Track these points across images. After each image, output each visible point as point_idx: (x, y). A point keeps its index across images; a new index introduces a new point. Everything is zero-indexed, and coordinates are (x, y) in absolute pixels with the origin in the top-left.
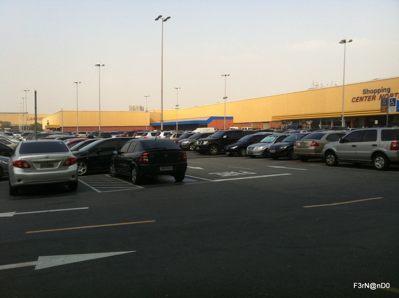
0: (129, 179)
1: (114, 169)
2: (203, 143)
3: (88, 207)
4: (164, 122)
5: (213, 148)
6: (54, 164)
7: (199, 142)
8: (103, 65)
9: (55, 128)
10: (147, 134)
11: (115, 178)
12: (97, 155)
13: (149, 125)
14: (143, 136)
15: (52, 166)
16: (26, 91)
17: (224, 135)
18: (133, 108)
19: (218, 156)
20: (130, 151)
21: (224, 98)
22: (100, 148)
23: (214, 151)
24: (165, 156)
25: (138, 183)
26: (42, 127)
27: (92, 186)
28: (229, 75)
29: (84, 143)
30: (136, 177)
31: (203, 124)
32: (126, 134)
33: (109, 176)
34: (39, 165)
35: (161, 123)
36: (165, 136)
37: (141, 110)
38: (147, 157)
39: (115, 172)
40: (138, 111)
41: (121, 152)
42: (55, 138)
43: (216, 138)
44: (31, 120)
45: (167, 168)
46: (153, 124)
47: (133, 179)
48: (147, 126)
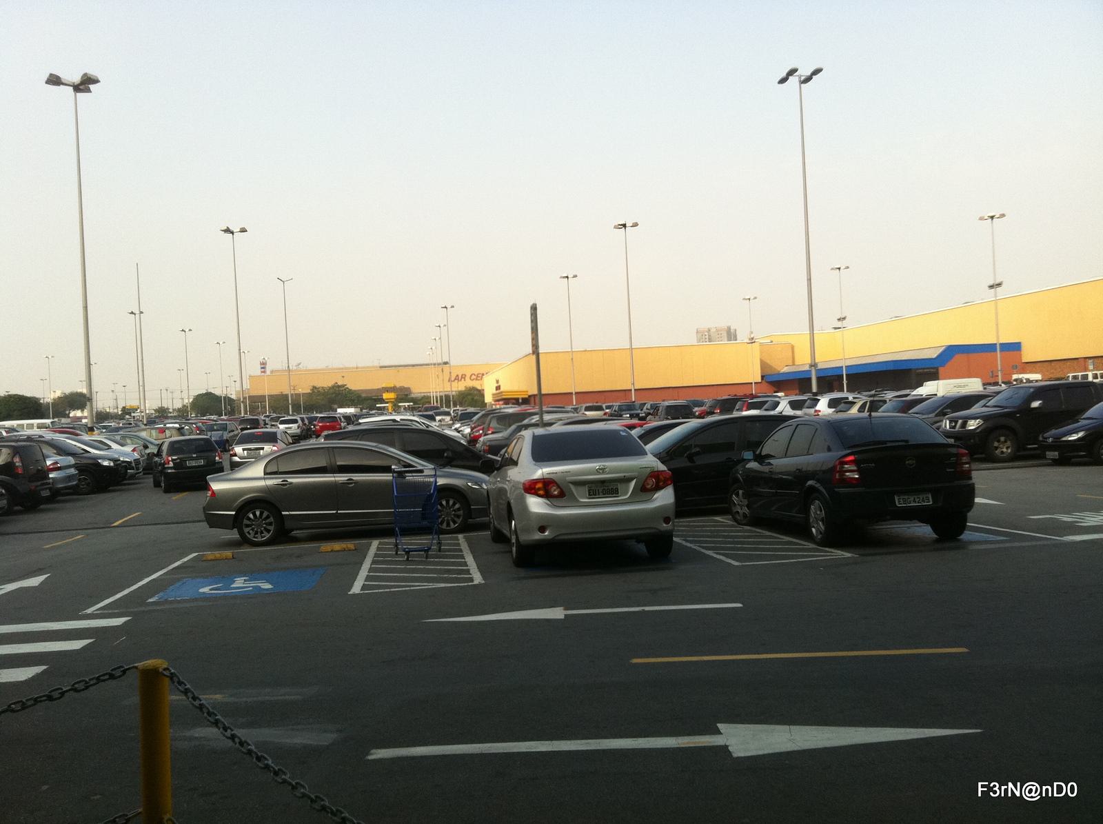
0: (800, 530)
1: (746, 502)
2: (964, 424)
3: (742, 604)
4: (820, 366)
5: (999, 441)
6: (619, 486)
7: (950, 423)
8: (635, 225)
9: (517, 400)
10: (777, 404)
11: (748, 528)
12: (689, 464)
13: (760, 381)
14: (766, 410)
15: (615, 492)
16: (446, 307)
17: (1034, 397)
18: (706, 333)
19: (1017, 464)
20: (782, 454)
21: (991, 287)
22: (696, 446)
23: (1005, 450)
24: (908, 464)
25: (830, 540)
26: (483, 396)
27: (703, 548)
28: (1003, 216)
29: (643, 432)
30: (823, 524)
31: (925, 370)
32: (713, 407)
33: (732, 523)
34: (586, 488)
35: (810, 371)
36: (833, 410)
37: (729, 339)
38: (855, 468)
39: (746, 510)
40: (721, 341)
41: (763, 453)
42: (555, 423)
43: (1006, 408)
44: (456, 381)
45: (917, 500)
46: (769, 375)
47: (814, 530)
48: (576, 393)
